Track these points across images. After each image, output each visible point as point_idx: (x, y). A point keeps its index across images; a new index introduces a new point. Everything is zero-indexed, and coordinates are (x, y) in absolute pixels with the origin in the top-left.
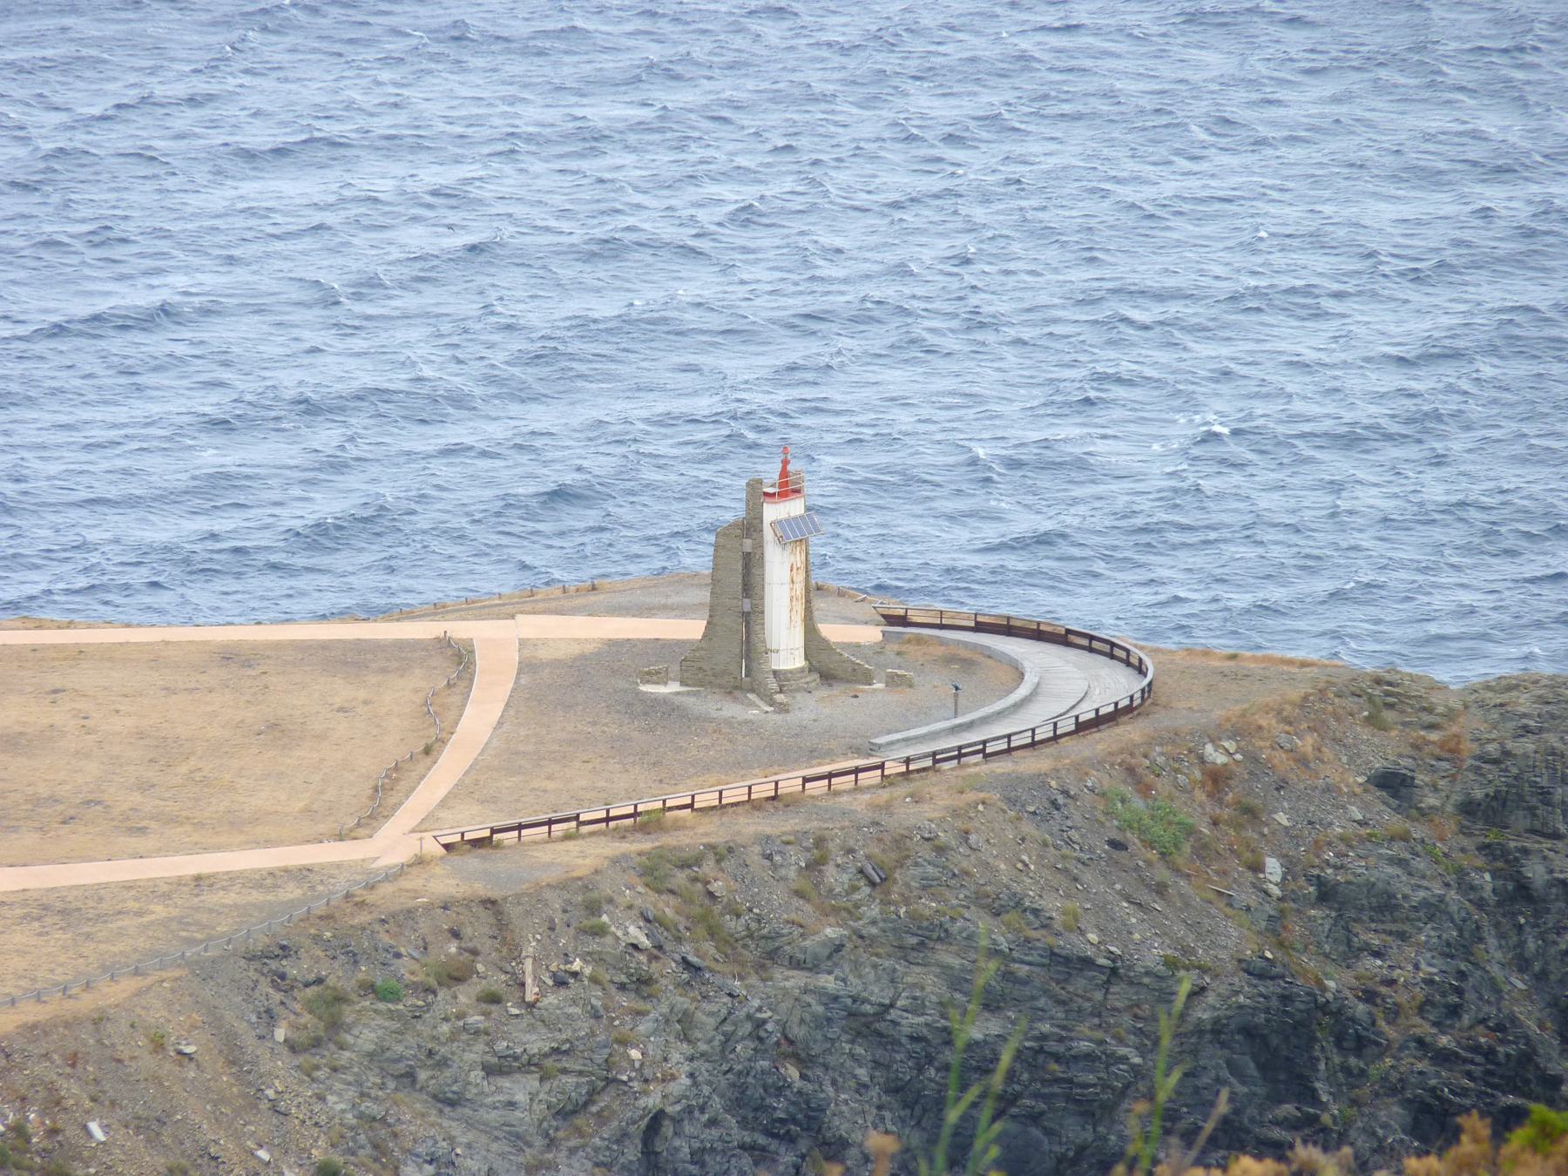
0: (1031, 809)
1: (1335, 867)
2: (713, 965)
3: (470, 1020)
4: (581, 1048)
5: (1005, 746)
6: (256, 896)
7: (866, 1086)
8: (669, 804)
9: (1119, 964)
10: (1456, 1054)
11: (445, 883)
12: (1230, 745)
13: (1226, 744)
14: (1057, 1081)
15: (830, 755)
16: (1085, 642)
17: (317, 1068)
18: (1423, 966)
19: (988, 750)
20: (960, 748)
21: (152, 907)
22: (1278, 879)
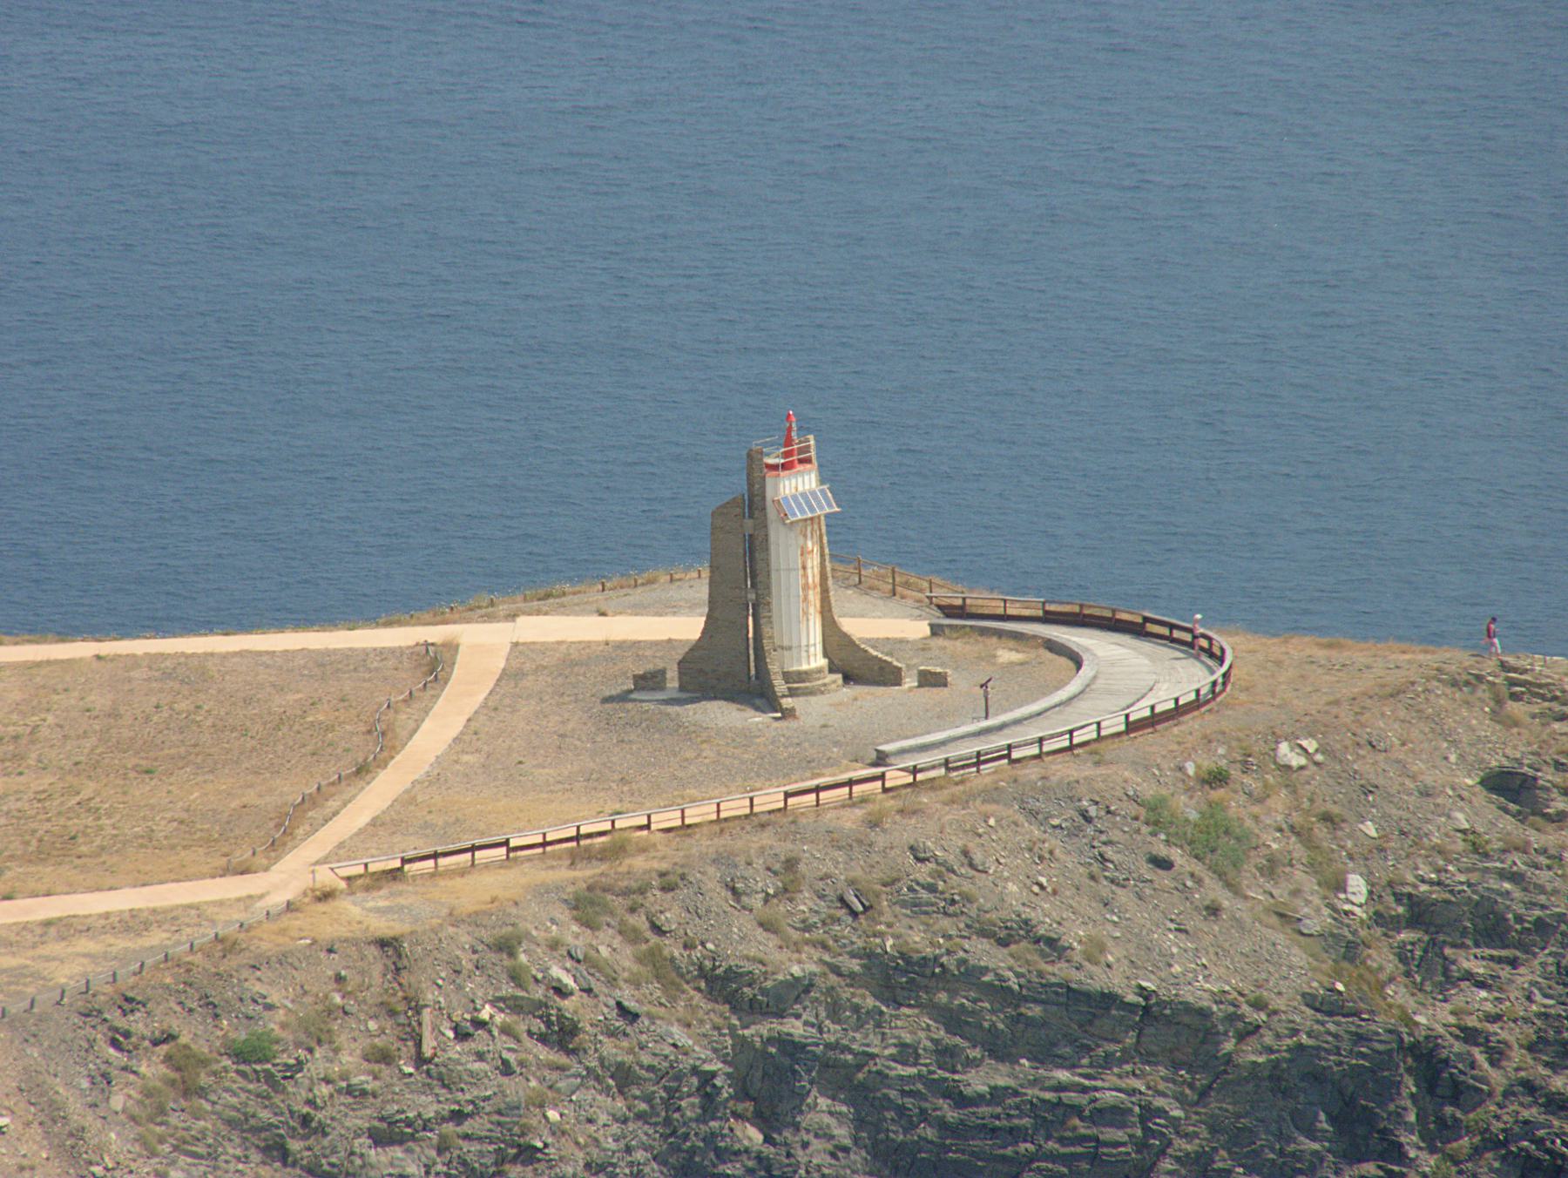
0: (1056, 822)
1: (1432, 883)
2: (654, 1010)
3: (355, 1081)
4: (488, 1109)
5: (1067, 743)
6: (121, 944)
7: (846, 1150)
9: (1153, 1001)
12: (1311, 745)
13: (1305, 743)
14: (1083, 1139)
15: (831, 763)
16: (1165, 631)
17: (161, 1141)
18: (1538, 997)
19: (503, 850)
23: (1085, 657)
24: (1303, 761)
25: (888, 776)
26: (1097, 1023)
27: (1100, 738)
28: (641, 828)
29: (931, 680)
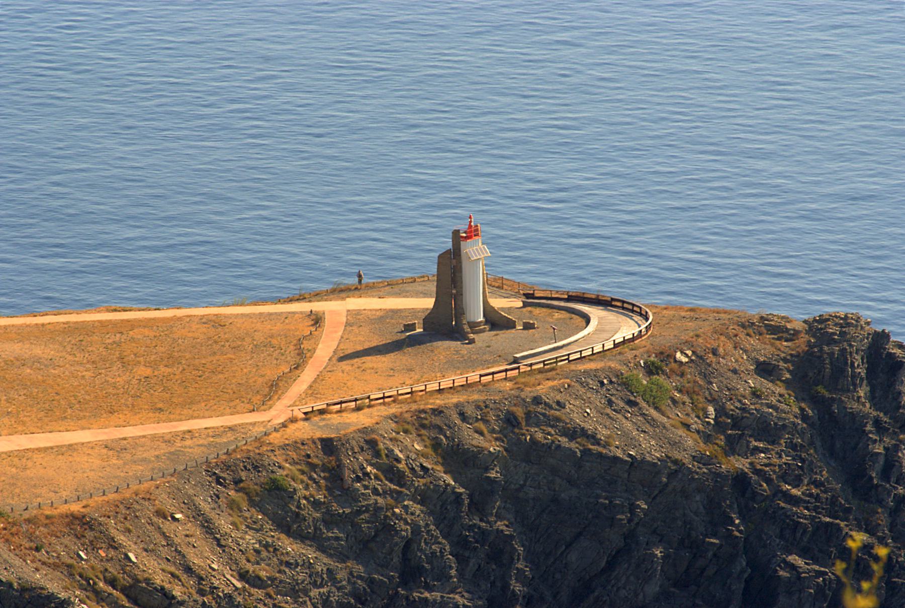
5: (579, 356)
8: (400, 392)
10: (801, 499)
11: (303, 431)
19: (570, 359)
20: (556, 358)
21: (854, 533)
22: (713, 417)
23: (591, 315)
24: (687, 360)
25: (521, 367)
26: (612, 469)
27: (593, 354)
28: (422, 391)
29: (528, 326)
